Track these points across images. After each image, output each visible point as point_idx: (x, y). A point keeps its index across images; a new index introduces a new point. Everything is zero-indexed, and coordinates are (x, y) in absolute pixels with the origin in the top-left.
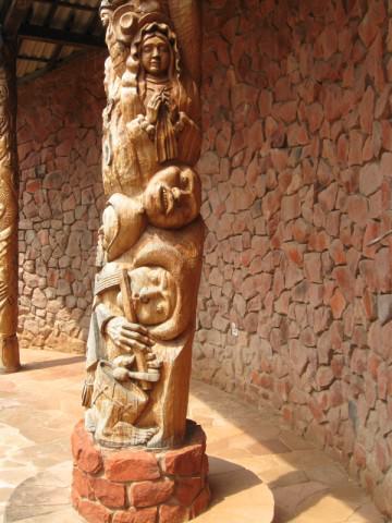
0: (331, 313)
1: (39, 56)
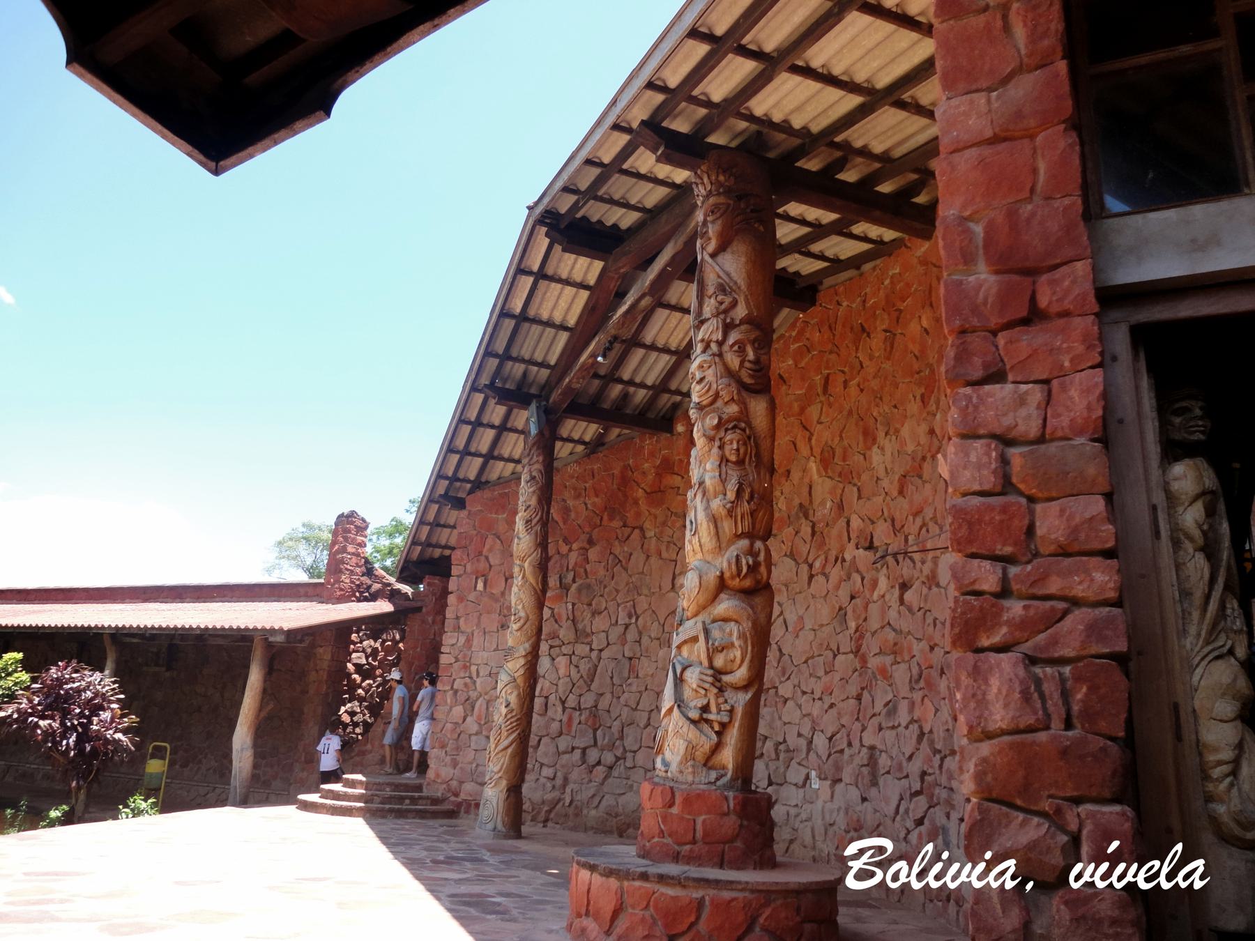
0: (921, 727)
1: (576, 438)
